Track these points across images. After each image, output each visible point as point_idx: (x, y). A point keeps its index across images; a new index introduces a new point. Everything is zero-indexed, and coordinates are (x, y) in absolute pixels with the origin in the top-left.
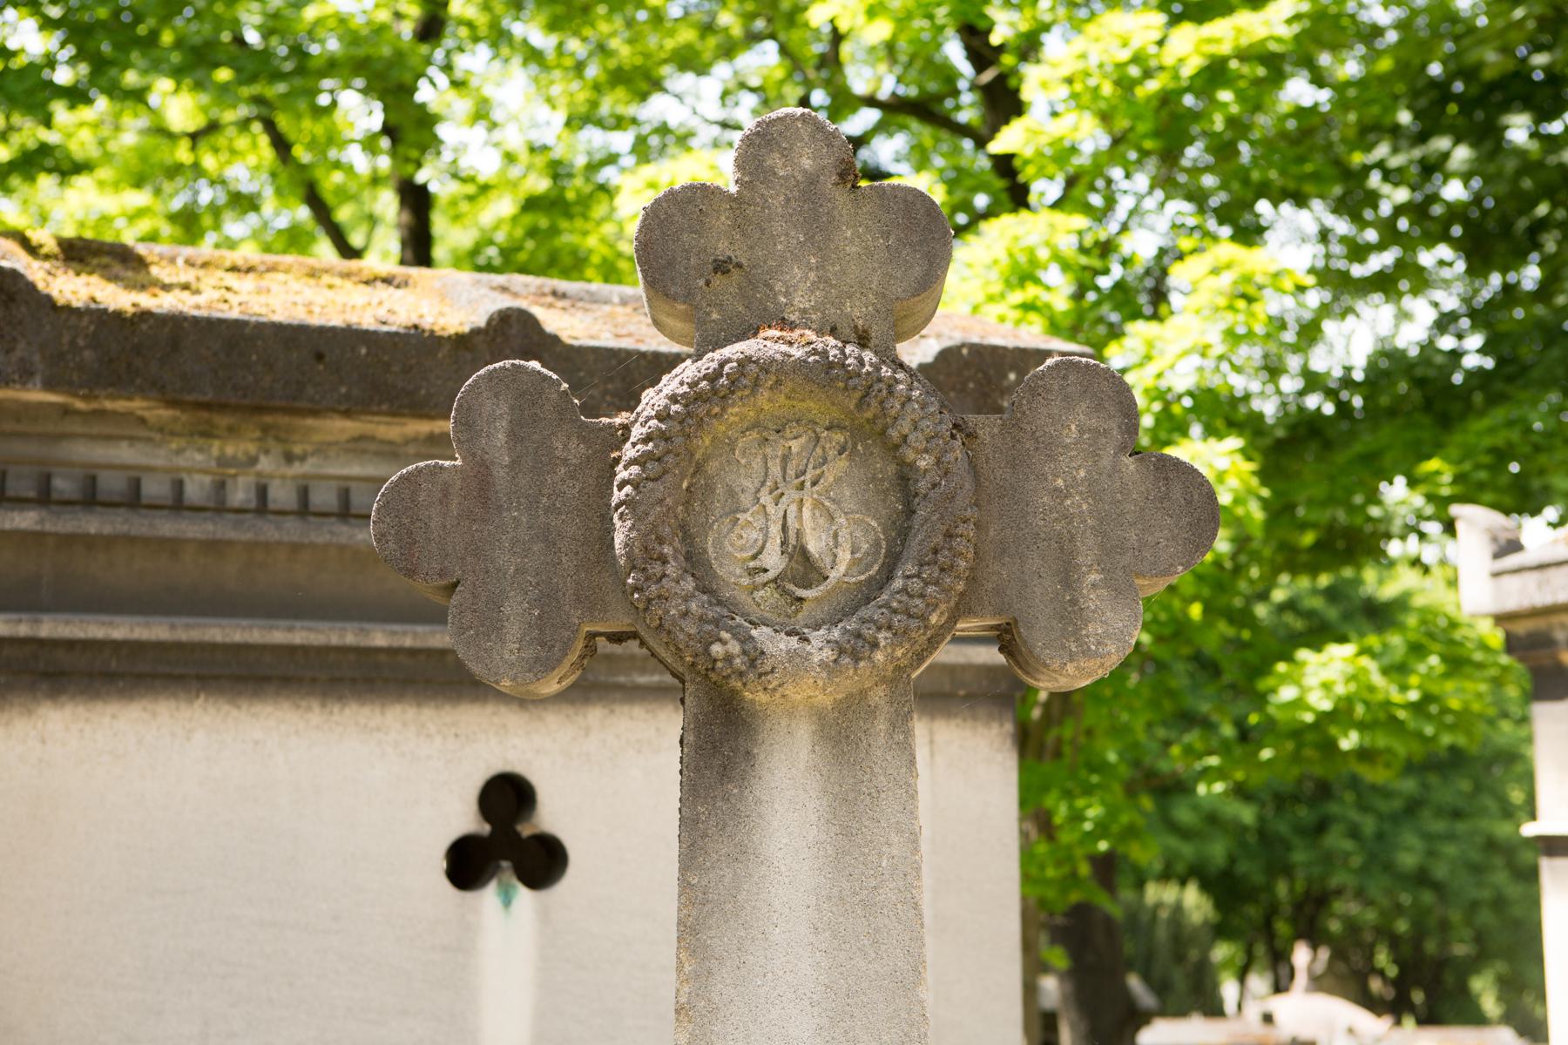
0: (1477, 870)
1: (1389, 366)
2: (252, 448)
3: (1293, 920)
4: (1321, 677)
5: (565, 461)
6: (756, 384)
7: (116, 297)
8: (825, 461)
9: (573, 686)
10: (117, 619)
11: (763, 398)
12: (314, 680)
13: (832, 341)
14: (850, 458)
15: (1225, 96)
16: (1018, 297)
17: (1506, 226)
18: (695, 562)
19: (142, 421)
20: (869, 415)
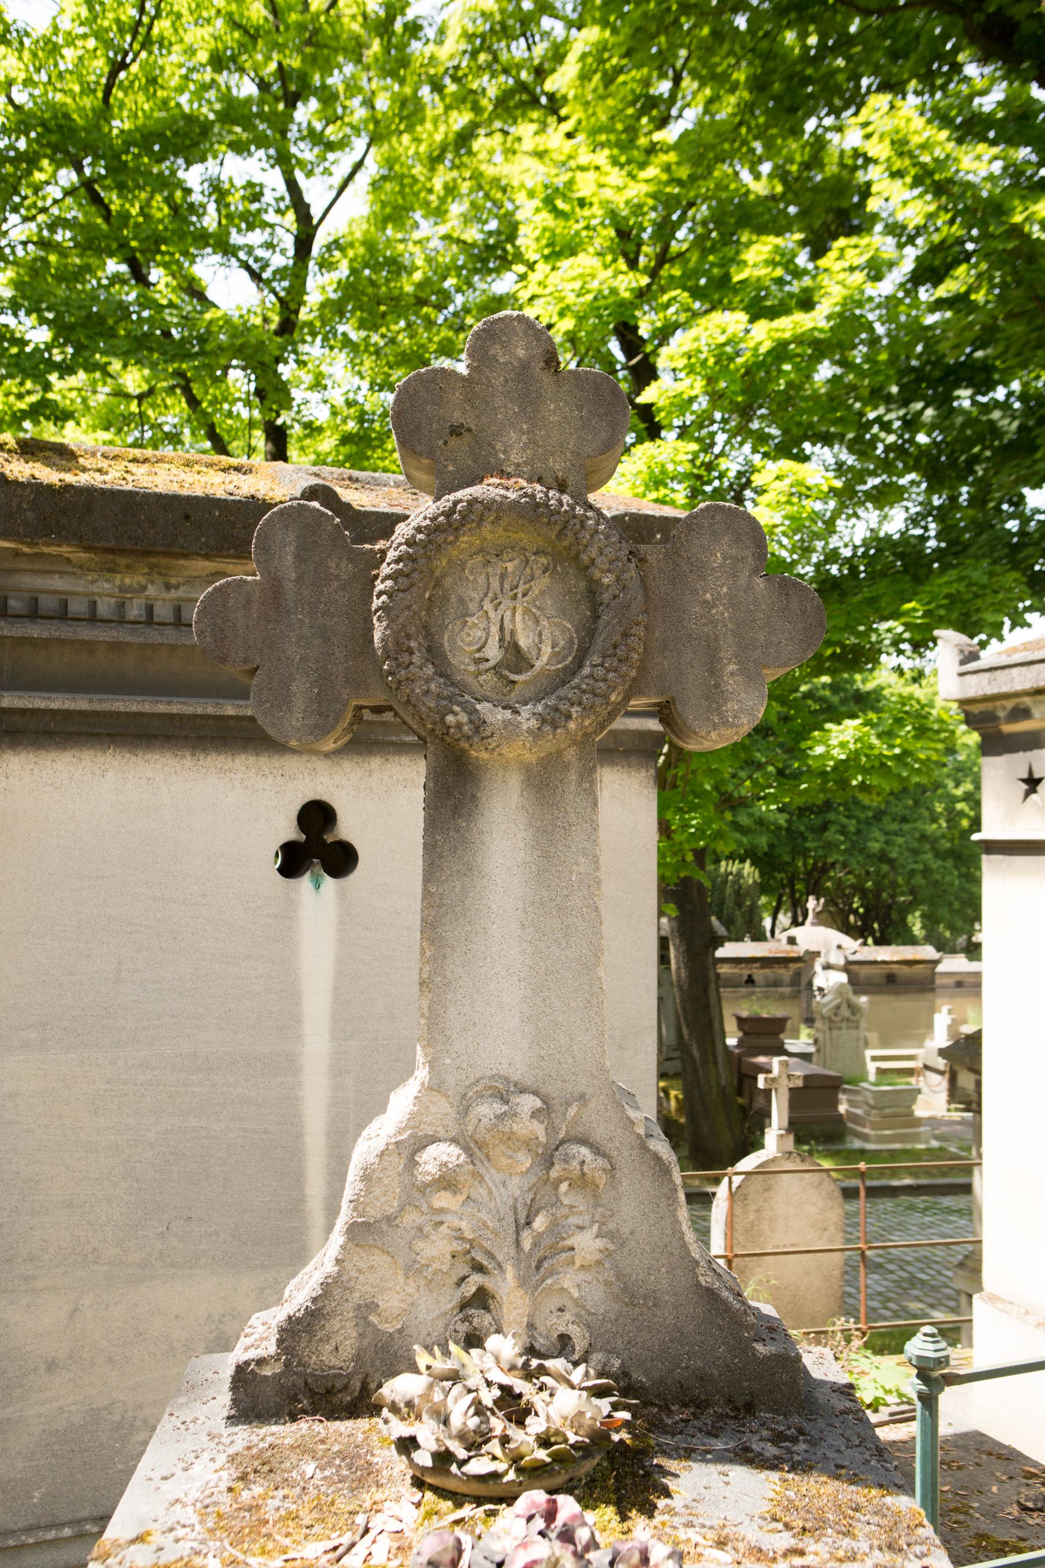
0: (915, 852)
1: (879, 544)
2: (143, 580)
3: (806, 881)
4: (841, 738)
5: (338, 577)
6: (481, 519)
7: (49, 475)
8: (533, 578)
9: (350, 742)
10: (53, 696)
11: (486, 529)
12: (186, 737)
13: (538, 487)
14: (552, 576)
15: (787, 367)
16: (654, 495)
17: (953, 462)
18: (434, 654)
19: (68, 560)
20: (566, 543)
